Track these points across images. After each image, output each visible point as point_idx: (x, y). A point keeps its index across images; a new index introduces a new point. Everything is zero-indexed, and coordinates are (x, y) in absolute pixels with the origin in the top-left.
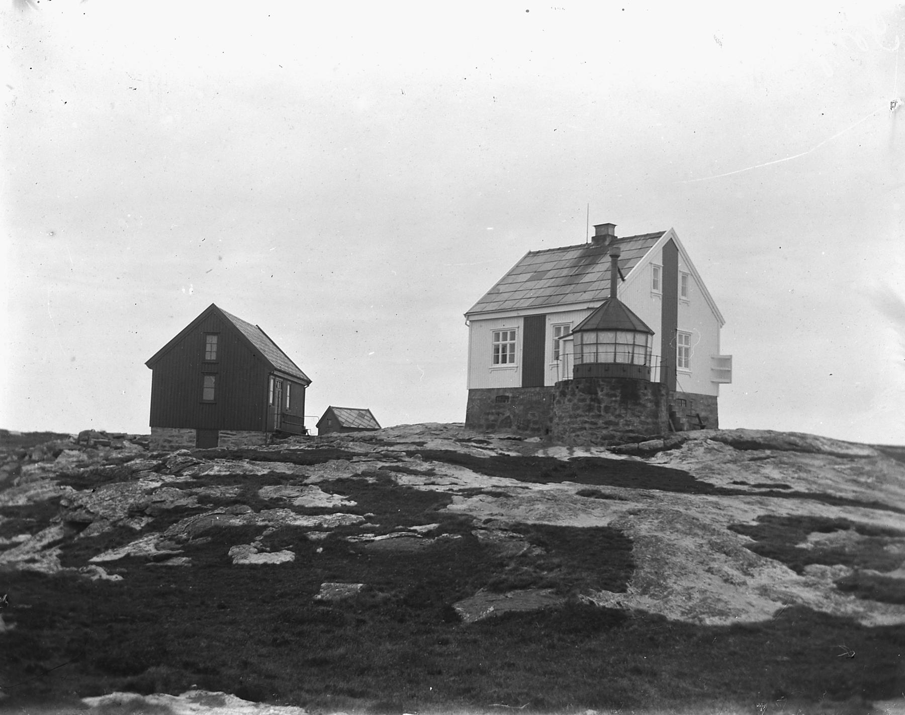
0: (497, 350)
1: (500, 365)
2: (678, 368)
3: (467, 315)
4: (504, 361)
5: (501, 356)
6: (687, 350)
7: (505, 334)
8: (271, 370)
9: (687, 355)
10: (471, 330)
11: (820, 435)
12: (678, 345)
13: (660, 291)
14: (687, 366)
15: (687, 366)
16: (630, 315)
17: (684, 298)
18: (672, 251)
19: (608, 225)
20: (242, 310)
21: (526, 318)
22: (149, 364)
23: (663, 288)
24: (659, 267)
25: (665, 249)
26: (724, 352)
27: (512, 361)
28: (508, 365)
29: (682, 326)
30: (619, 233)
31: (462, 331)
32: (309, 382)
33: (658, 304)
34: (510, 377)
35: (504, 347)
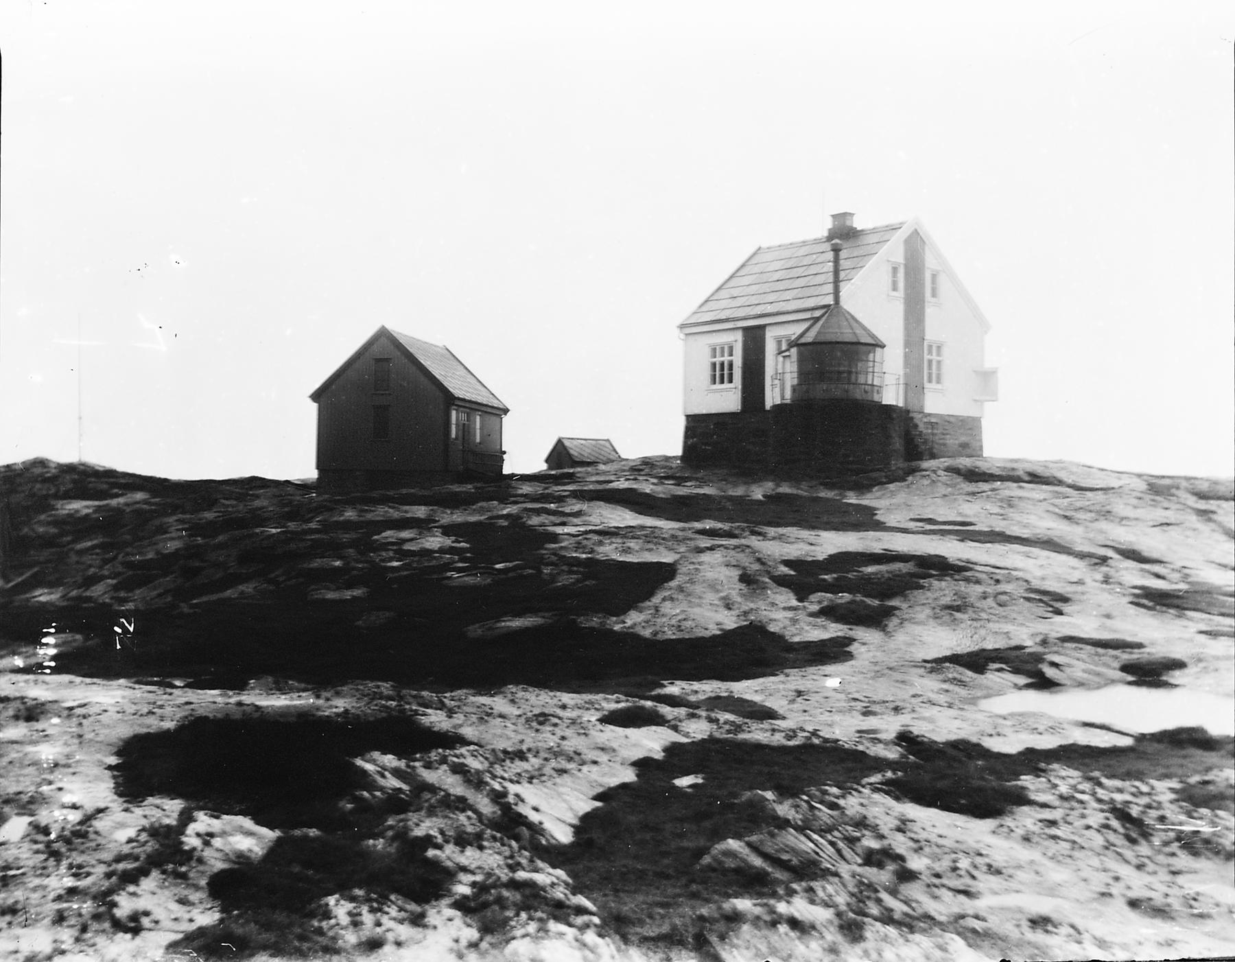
0: (714, 365)
1: (718, 386)
2: (927, 385)
3: (682, 326)
4: (722, 382)
5: (721, 374)
6: (939, 362)
7: (722, 349)
8: (450, 400)
9: (939, 368)
10: (817, 242)
11: (1182, 474)
12: (927, 357)
13: (901, 293)
14: (938, 382)
15: (938, 382)
16: (855, 325)
17: (934, 300)
18: (915, 245)
19: (845, 214)
20: (421, 330)
21: (745, 329)
22: (316, 396)
23: (906, 288)
24: (899, 264)
25: (908, 242)
26: (988, 365)
27: (731, 381)
28: (726, 385)
29: (931, 334)
30: (858, 224)
31: (676, 342)
32: (506, 411)
33: (899, 308)
34: (728, 399)
35: (722, 364)
